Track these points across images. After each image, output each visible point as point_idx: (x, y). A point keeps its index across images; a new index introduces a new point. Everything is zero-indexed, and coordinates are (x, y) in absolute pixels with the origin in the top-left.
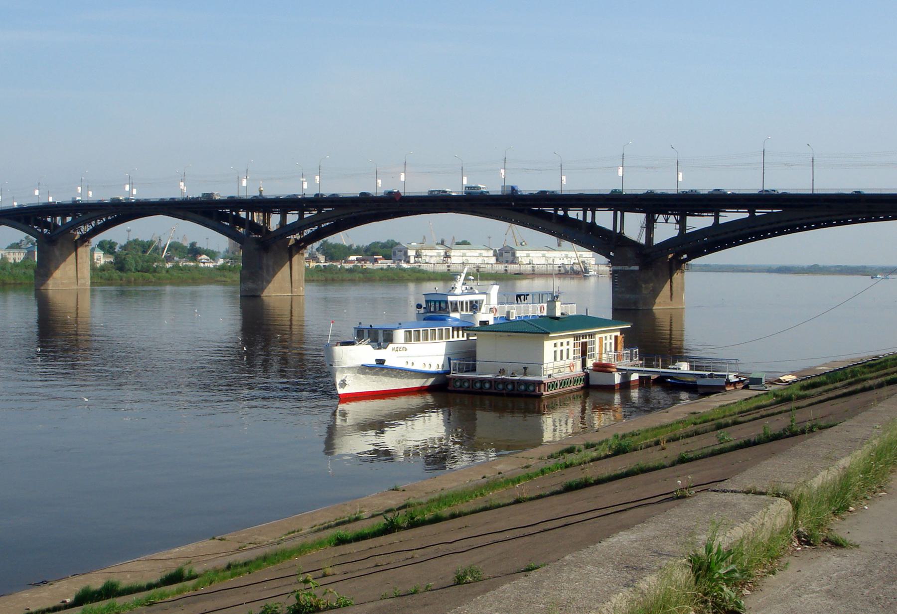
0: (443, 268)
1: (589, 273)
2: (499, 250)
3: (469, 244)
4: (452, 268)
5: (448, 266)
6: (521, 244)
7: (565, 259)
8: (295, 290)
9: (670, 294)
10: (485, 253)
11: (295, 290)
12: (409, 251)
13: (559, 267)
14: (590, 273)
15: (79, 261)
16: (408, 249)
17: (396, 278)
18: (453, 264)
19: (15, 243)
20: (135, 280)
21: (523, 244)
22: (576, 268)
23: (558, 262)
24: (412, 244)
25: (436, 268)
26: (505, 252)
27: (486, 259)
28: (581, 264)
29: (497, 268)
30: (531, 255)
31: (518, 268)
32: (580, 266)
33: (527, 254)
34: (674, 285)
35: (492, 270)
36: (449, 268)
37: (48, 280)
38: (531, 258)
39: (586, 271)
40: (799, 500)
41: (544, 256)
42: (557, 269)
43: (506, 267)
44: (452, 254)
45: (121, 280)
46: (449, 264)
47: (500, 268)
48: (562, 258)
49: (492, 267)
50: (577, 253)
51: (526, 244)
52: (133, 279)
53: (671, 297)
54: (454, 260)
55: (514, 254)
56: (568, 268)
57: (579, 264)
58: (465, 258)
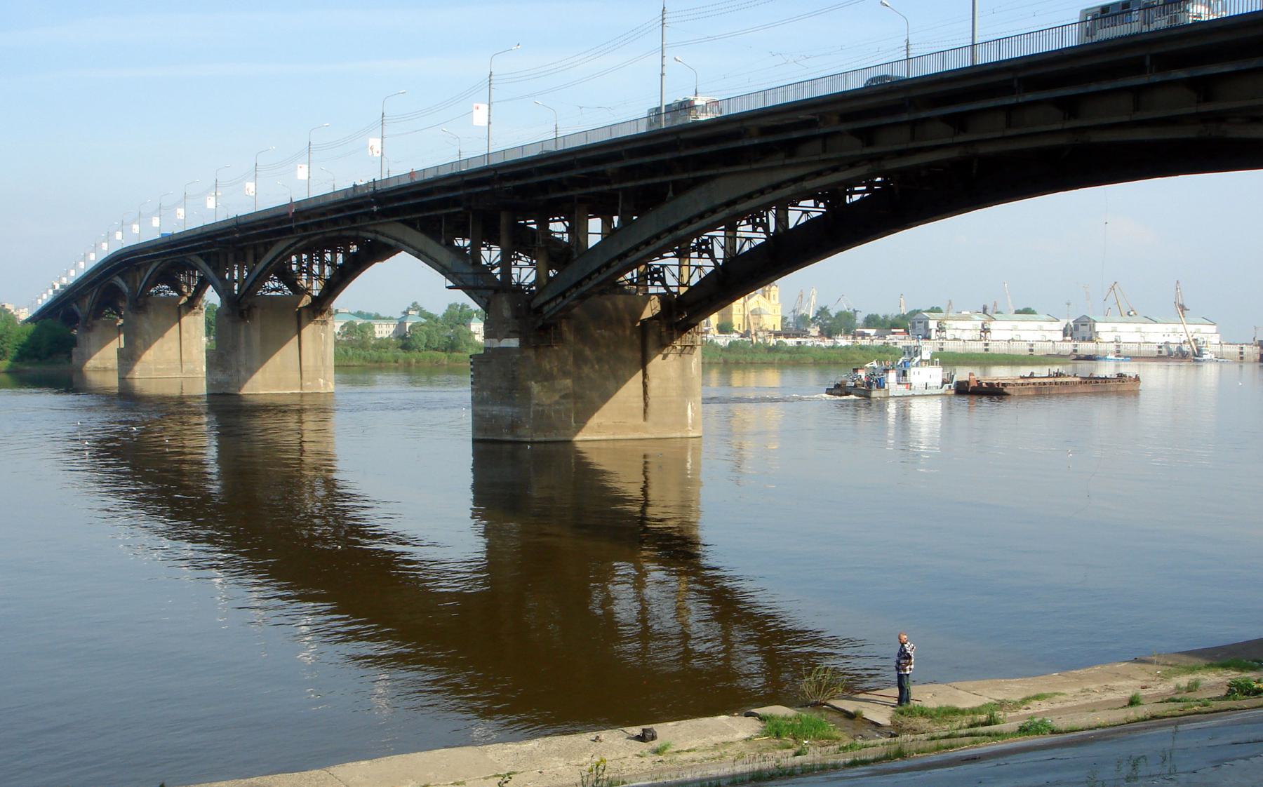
0: (978, 347)
1: (1202, 357)
2: (1073, 322)
3: (1033, 312)
4: (992, 348)
5: (987, 345)
6: (1128, 314)
7: (1171, 335)
8: (309, 383)
9: (642, 404)
10: (1047, 325)
11: (309, 383)
12: (930, 321)
13: (1160, 347)
14: (1205, 357)
15: (184, 335)
16: (928, 319)
17: (841, 360)
18: (992, 341)
19: (915, 310)
20: (418, 362)
21: (1132, 313)
22: (1185, 348)
23: (1161, 340)
24: (963, 313)
25: (967, 347)
26: (1082, 325)
27: (1047, 334)
28: (1193, 343)
29: (1062, 348)
30: (1118, 330)
31: (1094, 348)
32: (1191, 346)
33: (1137, 328)
34: (653, 384)
35: (1054, 350)
36: (987, 347)
37: (134, 365)
38: (1119, 334)
39: (1199, 352)
40: (1140, 704)
41: (1139, 331)
42: (1156, 349)
43: (1076, 345)
44: (991, 327)
45: (396, 362)
46: (987, 342)
47: (1067, 347)
48: (1166, 335)
49: (1053, 346)
50: (1187, 326)
51: (1135, 314)
52: (414, 360)
53: (645, 412)
54: (993, 335)
55: (1092, 328)
56: (1174, 348)
57: (1190, 343)
58: (1014, 333)
